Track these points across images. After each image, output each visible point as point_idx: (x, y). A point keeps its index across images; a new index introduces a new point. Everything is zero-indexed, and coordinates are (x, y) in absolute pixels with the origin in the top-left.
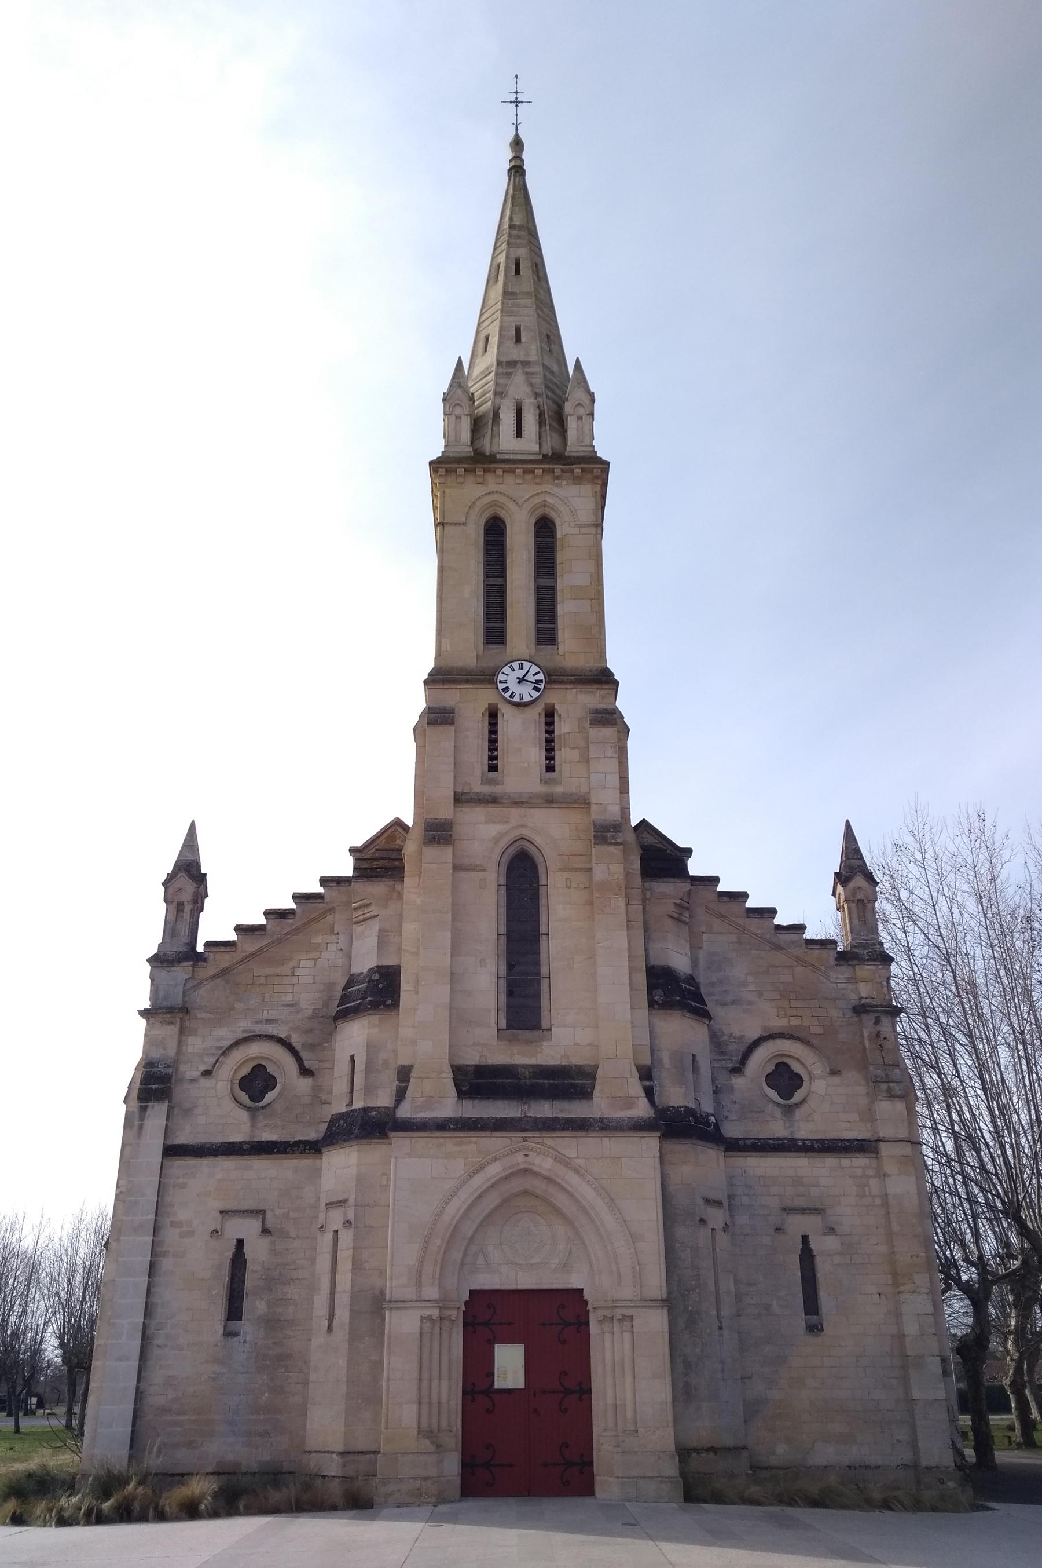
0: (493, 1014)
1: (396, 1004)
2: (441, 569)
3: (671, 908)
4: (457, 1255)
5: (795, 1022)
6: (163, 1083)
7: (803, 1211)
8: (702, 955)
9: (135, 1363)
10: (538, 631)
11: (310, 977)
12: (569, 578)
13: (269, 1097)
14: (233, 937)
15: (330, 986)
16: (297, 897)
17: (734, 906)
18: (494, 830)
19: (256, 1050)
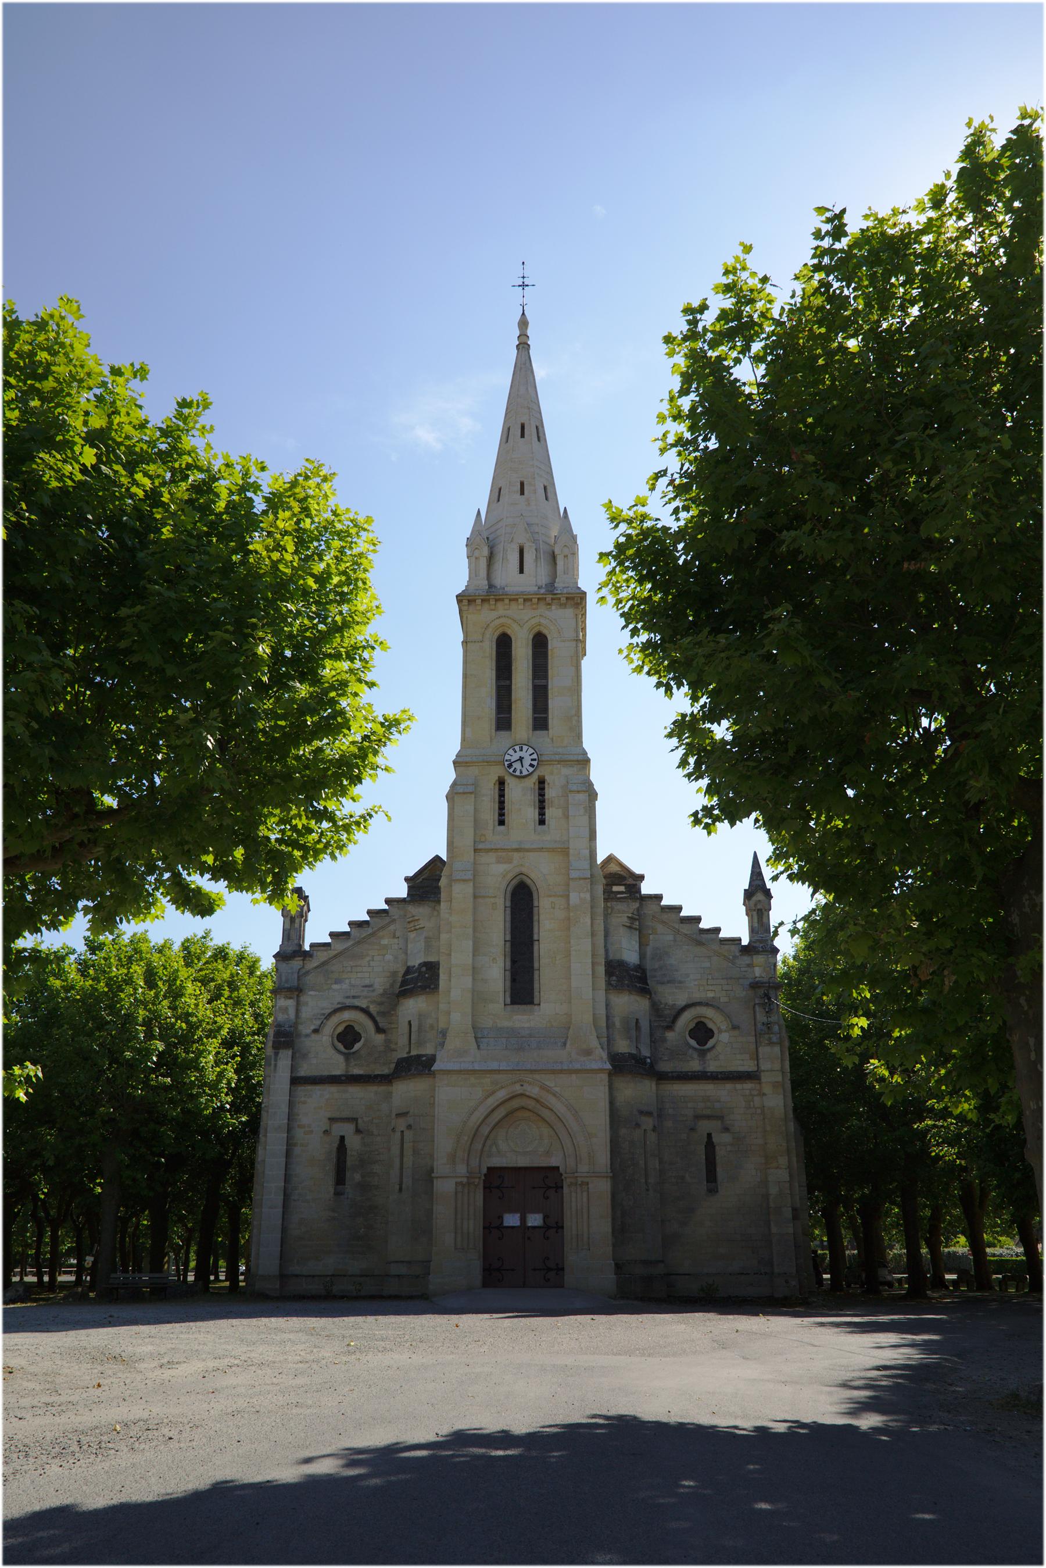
0: (501, 994)
1: (437, 987)
2: (465, 676)
3: (624, 920)
4: (478, 1146)
5: (710, 995)
6: (990, 185)
7: (709, 1117)
8: (649, 950)
9: (281, 1210)
10: (535, 719)
11: (375, 971)
12: (556, 681)
13: (357, 1046)
14: (328, 940)
15: (394, 974)
16: (370, 912)
17: (672, 916)
18: (502, 868)
19: (347, 1015)
